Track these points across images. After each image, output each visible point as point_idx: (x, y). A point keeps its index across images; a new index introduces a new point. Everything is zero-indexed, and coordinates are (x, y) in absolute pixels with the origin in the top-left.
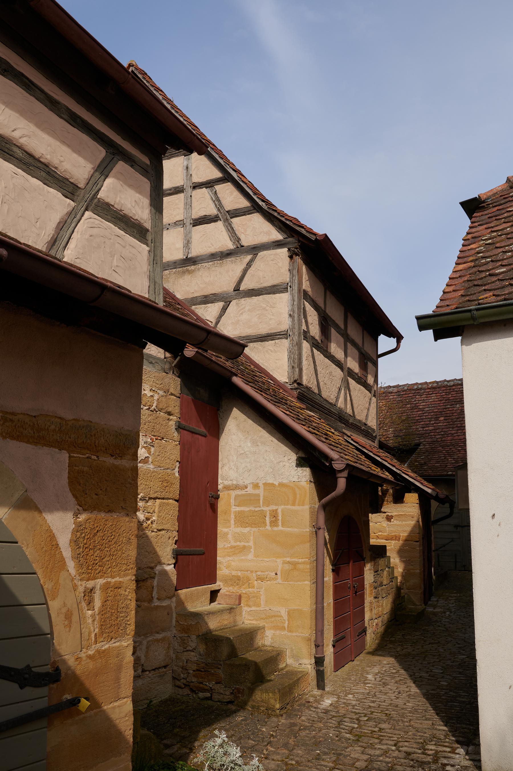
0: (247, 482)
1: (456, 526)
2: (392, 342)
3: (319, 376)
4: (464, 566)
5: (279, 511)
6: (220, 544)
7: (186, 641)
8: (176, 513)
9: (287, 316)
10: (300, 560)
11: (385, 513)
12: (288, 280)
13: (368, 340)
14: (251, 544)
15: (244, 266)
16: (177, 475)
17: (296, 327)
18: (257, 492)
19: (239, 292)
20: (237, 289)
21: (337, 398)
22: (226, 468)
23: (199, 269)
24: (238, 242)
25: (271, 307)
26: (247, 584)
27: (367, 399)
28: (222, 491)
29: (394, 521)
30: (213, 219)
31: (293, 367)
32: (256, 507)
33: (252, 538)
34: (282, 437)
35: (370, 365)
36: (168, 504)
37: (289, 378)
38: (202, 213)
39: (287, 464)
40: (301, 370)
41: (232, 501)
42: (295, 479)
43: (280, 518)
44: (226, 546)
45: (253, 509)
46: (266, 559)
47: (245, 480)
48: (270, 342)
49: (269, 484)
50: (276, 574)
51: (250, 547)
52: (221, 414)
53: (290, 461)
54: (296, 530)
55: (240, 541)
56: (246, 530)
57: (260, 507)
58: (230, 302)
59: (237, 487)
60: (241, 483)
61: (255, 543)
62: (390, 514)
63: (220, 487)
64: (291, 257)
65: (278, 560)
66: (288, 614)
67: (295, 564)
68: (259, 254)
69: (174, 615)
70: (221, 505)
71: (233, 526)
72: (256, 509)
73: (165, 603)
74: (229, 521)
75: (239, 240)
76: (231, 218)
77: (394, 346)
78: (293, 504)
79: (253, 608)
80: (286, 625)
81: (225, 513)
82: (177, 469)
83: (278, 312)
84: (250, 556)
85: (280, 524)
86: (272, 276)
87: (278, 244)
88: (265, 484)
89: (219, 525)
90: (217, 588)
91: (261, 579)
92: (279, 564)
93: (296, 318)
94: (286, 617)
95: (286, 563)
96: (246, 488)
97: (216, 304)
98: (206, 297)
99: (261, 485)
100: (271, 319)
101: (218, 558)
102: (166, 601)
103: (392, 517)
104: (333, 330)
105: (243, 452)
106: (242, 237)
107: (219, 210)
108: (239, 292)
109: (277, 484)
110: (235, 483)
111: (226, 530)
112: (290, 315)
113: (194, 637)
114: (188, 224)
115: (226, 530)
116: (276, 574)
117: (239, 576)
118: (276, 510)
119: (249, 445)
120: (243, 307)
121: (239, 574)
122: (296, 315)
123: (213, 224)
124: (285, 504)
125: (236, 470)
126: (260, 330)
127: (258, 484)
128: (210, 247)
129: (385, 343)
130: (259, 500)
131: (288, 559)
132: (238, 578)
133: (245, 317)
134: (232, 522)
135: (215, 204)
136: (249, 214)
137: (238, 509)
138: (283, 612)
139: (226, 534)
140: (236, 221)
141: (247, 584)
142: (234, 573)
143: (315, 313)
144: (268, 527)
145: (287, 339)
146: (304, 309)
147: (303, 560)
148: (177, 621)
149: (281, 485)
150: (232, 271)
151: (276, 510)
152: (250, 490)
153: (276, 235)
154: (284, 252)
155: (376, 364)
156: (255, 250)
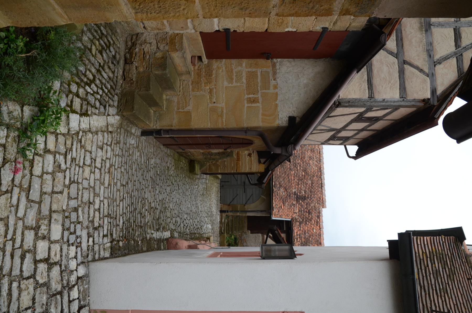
0: (278, 80)
1: (244, 183)
2: (353, 154)
3: (341, 117)
4: (223, 186)
5: (258, 104)
6: (234, 61)
7: (164, 42)
8: (257, 30)
9: (384, 98)
10: (224, 120)
11: (253, 152)
12: (408, 98)
13: (357, 141)
14: (235, 84)
15: (420, 66)
16: (287, 30)
17: (376, 104)
18: (272, 88)
19: (404, 63)
20: (405, 62)
21: (323, 126)
22: (288, 64)
23: (422, 34)
24: (439, 63)
25: (391, 87)
26: (207, 81)
27: (320, 140)
28: (271, 62)
29: (248, 158)
30: (457, 45)
31: (349, 102)
32: (260, 87)
33: (239, 84)
34: (310, 106)
35: (341, 142)
36: (264, 24)
37: (342, 99)
38: (463, 35)
39: (291, 110)
40: (346, 107)
41: (265, 69)
42: (280, 116)
43: (253, 105)
44: (232, 66)
45: (259, 85)
46: (224, 95)
47: (279, 78)
48: (367, 86)
49: (277, 97)
50: (214, 103)
51: (232, 84)
52: (327, 60)
53: (293, 112)
54: (245, 117)
55: (236, 76)
56: (244, 80)
57: (261, 90)
58: (396, 58)
59: (275, 73)
60: (278, 75)
61: (235, 87)
62: (252, 155)
63: (275, 60)
64: (424, 100)
65: (224, 104)
66: (188, 112)
67: (222, 116)
68: (428, 78)
69: (181, 32)
70: (261, 61)
71: (247, 70)
72: (259, 88)
73: (189, 24)
74: (250, 67)
75: (440, 63)
76: (457, 57)
77: (351, 155)
78: (263, 115)
79: (191, 87)
80: (180, 110)
81: (256, 64)
82: (290, 29)
83: (388, 91)
84: (226, 84)
85: (249, 105)
86: (412, 87)
87: (434, 91)
88: (277, 94)
89: (248, 60)
90: (203, 60)
91: (211, 91)
92: (222, 105)
93: (382, 104)
94: (186, 110)
95: (222, 110)
96: (274, 80)
97: (396, 47)
98: (402, 39)
99: (276, 90)
100: (382, 86)
101: (224, 60)
102: (191, 25)
103: (251, 157)
104: (368, 124)
105: (300, 77)
106: (441, 66)
107: (464, 48)
108: (404, 63)
109: (276, 103)
110: (278, 71)
111: (244, 65)
112: (384, 100)
113: (167, 48)
114: (456, 24)
115: (244, 65)
116: (214, 103)
117: (212, 76)
118: (259, 102)
119: (305, 82)
120: (393, 67)
121: (213, 76)
122: (384, 104)
123: (454, 44)
124: (262, 108)
125: (287, 71)
126: (375, 79)
127: (277, 88)
128: (437, 42)
129: (353, 150)
130: (266, 89)
131: (225, 111)
132: (210, 75)
133: (385, 69)
134: (250, 70)
135: (469, 45)
136: (458, 70)
137: (259, 74)
138: (189, 108)
139: (241, 65)
140: (454, 60)
141: (207, 81)
142: (214, 72)
143: (382, 115)
144: (246, 96)
145: (369, 98)
146: (387, 109)
147: (224, 122)
148: (177, 34)
149: (276, 106)
150: (418, 59)
151: (259, 102)
152: (273, 82)
153: (440, 90)
154: (428, 95)
155: (341, 144)
156: (432, 76)
